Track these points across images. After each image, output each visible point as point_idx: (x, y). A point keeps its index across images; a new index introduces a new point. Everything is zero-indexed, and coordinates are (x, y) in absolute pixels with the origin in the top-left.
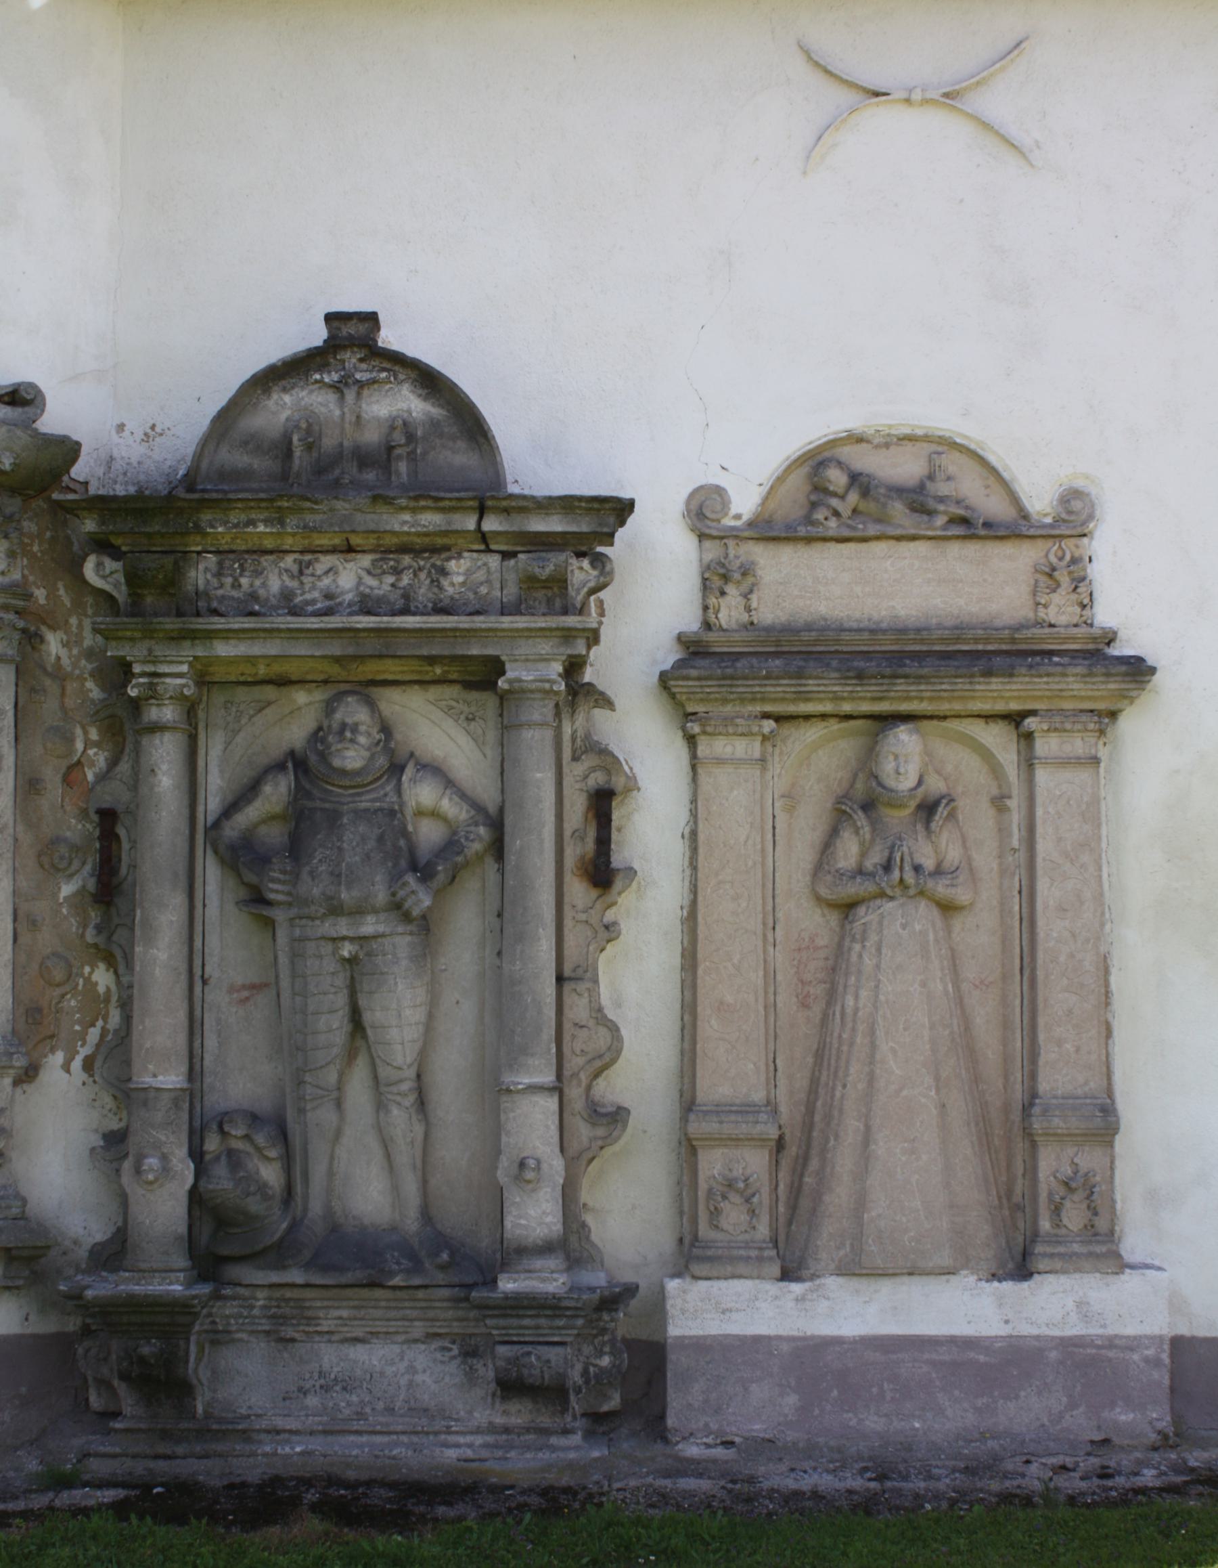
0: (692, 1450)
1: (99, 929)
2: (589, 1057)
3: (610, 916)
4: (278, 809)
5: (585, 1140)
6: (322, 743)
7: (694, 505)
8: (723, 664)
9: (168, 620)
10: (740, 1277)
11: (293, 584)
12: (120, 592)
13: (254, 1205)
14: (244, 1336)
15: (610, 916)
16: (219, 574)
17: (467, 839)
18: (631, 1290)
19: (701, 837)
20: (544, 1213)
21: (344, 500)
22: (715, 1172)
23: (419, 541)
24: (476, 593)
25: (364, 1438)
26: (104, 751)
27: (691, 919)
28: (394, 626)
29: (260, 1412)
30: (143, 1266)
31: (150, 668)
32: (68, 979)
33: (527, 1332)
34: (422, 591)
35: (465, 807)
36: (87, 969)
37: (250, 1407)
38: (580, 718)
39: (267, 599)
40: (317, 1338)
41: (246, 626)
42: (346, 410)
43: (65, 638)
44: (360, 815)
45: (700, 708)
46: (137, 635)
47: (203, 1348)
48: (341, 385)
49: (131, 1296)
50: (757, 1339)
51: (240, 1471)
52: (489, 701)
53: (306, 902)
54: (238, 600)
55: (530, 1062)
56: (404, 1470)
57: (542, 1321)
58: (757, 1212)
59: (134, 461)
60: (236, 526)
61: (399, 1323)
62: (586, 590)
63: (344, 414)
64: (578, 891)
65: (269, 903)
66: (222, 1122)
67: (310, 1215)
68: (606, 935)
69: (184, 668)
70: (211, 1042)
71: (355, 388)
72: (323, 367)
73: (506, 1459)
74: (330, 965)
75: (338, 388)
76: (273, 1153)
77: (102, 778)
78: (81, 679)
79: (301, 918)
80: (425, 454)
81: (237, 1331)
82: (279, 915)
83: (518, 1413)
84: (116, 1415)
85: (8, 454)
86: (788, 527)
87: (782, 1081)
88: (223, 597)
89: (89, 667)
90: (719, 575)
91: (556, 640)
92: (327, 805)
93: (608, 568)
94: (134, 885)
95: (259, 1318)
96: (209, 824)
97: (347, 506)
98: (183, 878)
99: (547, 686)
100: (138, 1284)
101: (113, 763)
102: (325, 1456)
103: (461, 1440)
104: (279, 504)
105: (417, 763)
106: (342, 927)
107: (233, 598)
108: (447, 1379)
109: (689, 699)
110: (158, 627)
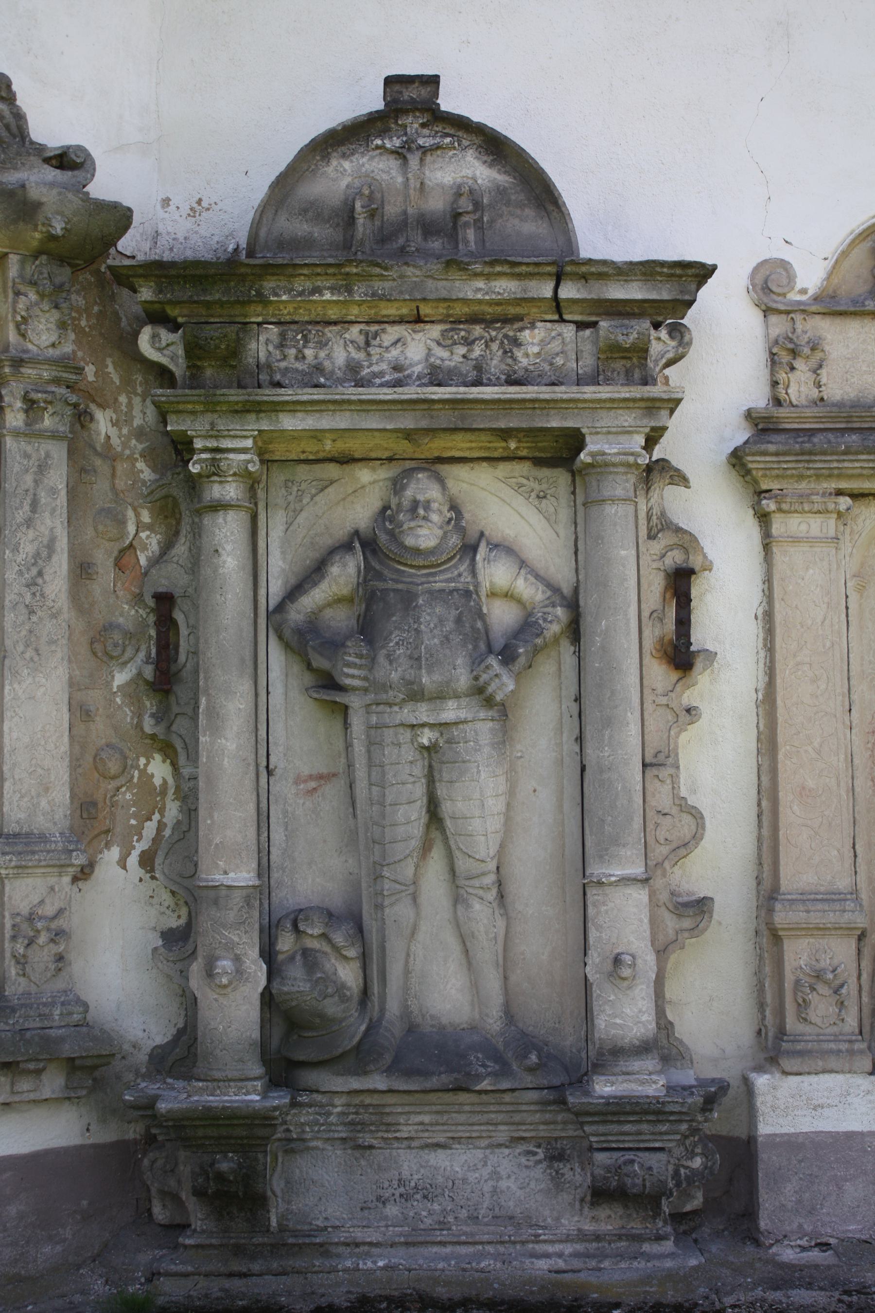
0: (788, 1254)
1: (158, 718)
2: (674, 845)
3: (690, 697)
4: (345, 591)
5: (671, 932)
6: (391, 522)
7: (759, 280)
8: (800, 440)
9: (232, 391)
10: (831, 1071)
11: (360, 356)
12: (177, 365)
13: (332, 1008)
14: (319, 1144)
15: (690, 697)
16: (281, 346)
17: (545, 620)
18: (723, 1087)
19: (778, 618)
20: (640, 1011)
21: (414, 266)
22: (802, 963)
23: (490, 310)
24: (551, 364)
25: (448, 1249)
26: (156, 533)
27: (768, 700)
28: (471, 396)
29: (338, 1224)
30: (217, 1075)
31: (212, 444)
32: (123, 772)
33: (627, 1138)
34: (494, 362)
35: (541, 587)
36: (142, 761)
37: (326, 1219)
38: (655, 495)
39: (332, 372)
40: (396, 1145)
41: (315, 397)
42: (410, 175)
43: (114, 417)
44: (436, 595)
45: (775, 485)
47: (277, 1159)
48: (404, 151)
49: (208, 1109)
50: (850, 1136)
51: (322, 1291)
52: (561, 477)
53: (385, 687)
54: (303, 373)
55: (622, 852)
56: (496, 1286)
57: (645, 1127)
58: (846, 1003)
59: (180, 236)
60: (301, 294)
61: (482, 1128)
62: (664, 361)
63: (407, 179)
64: (660, 674)
65: (341, 688)
66: (296, 920)
67: (388, 1015)
68: (688, 717)
69: (249, 443)
70: (278, 835)
71: (418, 154)
72: (384, 132)
73: (600, 1269)
74: (408, 753)
75: (400, 154)
76: (352, 953)
77: (157, 561)
78: (132, 460)
79: (378, 704)
80: (492, 221)
81: (312, 1139)
82: (355, 701)
83: (608, 1220)
84: (183, 1227)
85: (59, 218)
86: (854, 302)
87: (862, 868)
88: (286, 369)
89: (140, 447)
90: (788, 349)
91: (640, 412)
92: (400, 586)
93: (686, 338)
94: (196, 671)
95: (337, 1125)
96: (271, 609)
97: (418, 273)
98: (249, 663)
99: (631, 459)
100: (212, 1095)
101: (167, 547)
102: (410, 1271)
103: (550, 1249)
104: (347, 269)
105: (488, 543)
106: (422, 713)
107: (297, 370)
108: (533, 1185)
109: (765, 476)
110: (222, 399)
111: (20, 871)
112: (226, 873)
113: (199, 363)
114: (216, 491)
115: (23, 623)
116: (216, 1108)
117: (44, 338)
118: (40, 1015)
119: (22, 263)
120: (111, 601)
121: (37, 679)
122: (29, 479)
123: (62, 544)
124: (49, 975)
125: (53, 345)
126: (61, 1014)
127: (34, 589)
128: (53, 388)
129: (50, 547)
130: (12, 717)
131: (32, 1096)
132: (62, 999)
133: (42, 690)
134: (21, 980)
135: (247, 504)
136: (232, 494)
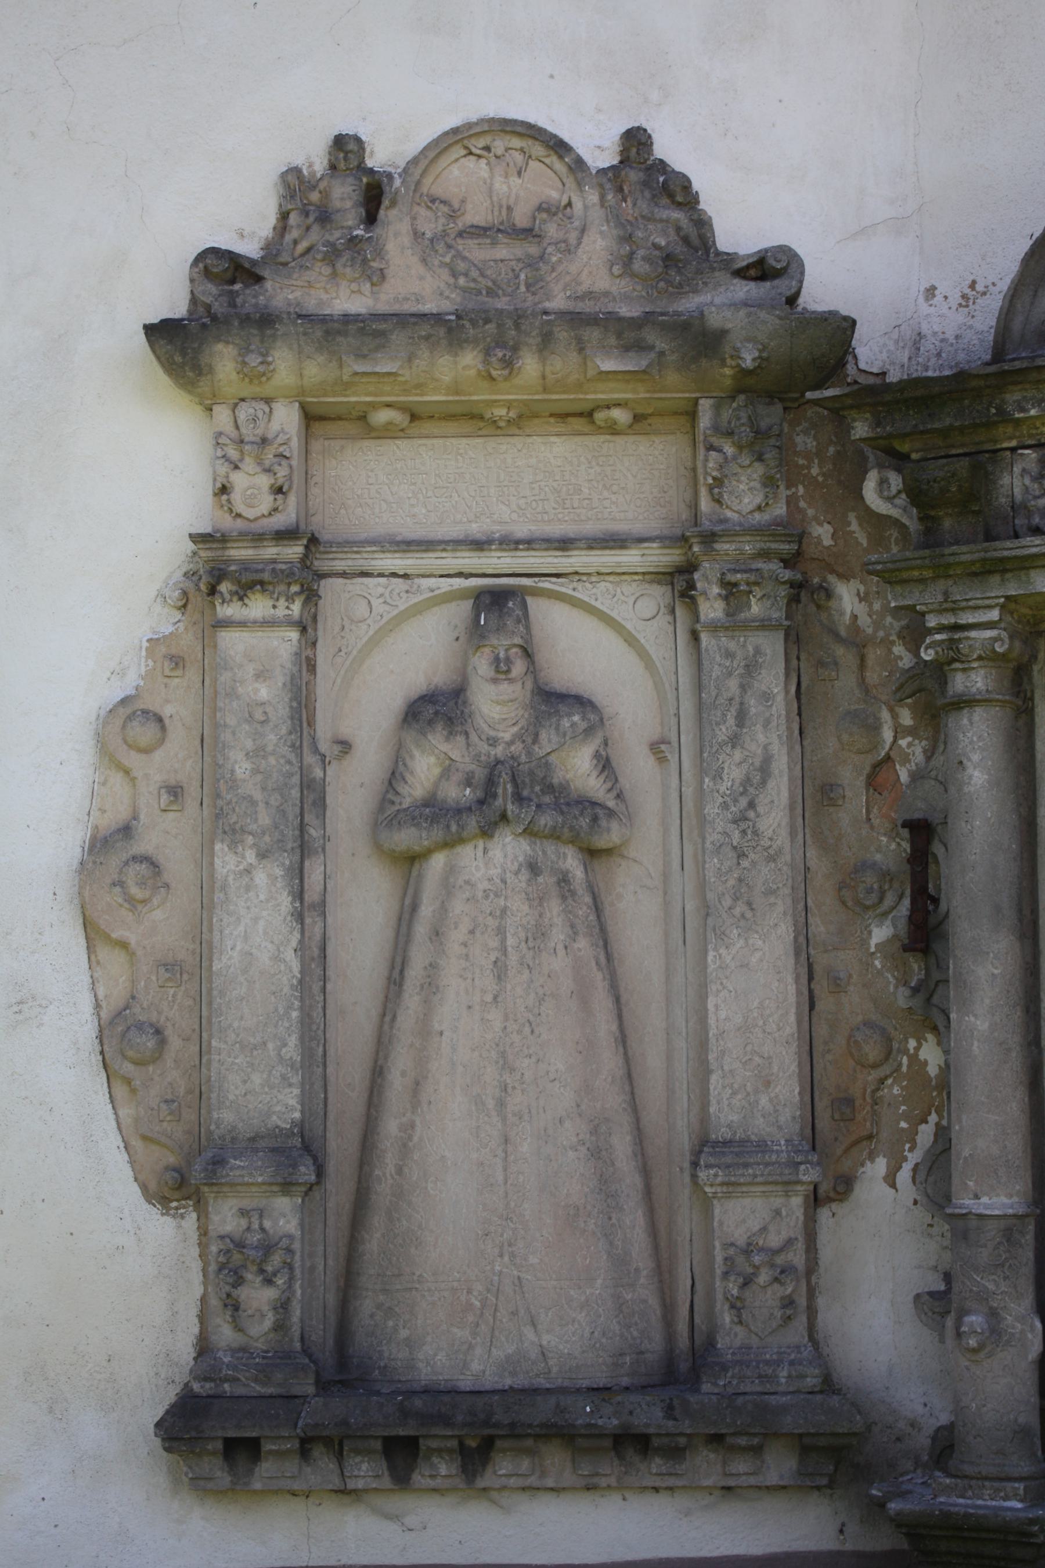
12: (911, 518)
30: (968, 1469)
31: (948, 619)
36: (912, 1044)
43: (862, 588)
46: (928, 574)
49: (947, 1515)
59: (950, 335)
69: (994, 615)
89: (897, 625)
100: (963, 1497)
110: (951, 559)
111: (731, 1189)
112: (977, 1197)
113: (933, 513)
114: (960, 683)
115: (731, 870)
116: (957, 1514)
117: (746, 500)
118: (760, 1376)
119: (717, 408)
120: (864, 832)
121: (751, 942)
122: (733, 685)
123: (781, 763)
124: (774, 1325)
125: (759, 508)
126: (789, 1377)
127: (743, 825)
128: (760, 565)
129: (765, 770)
130: (718, 991)
131: (752, 1481)
132: (793, 1356)
133: (758, 955)
134: (738, 1329)
135: (1000, 697)
136: (979, 685)
